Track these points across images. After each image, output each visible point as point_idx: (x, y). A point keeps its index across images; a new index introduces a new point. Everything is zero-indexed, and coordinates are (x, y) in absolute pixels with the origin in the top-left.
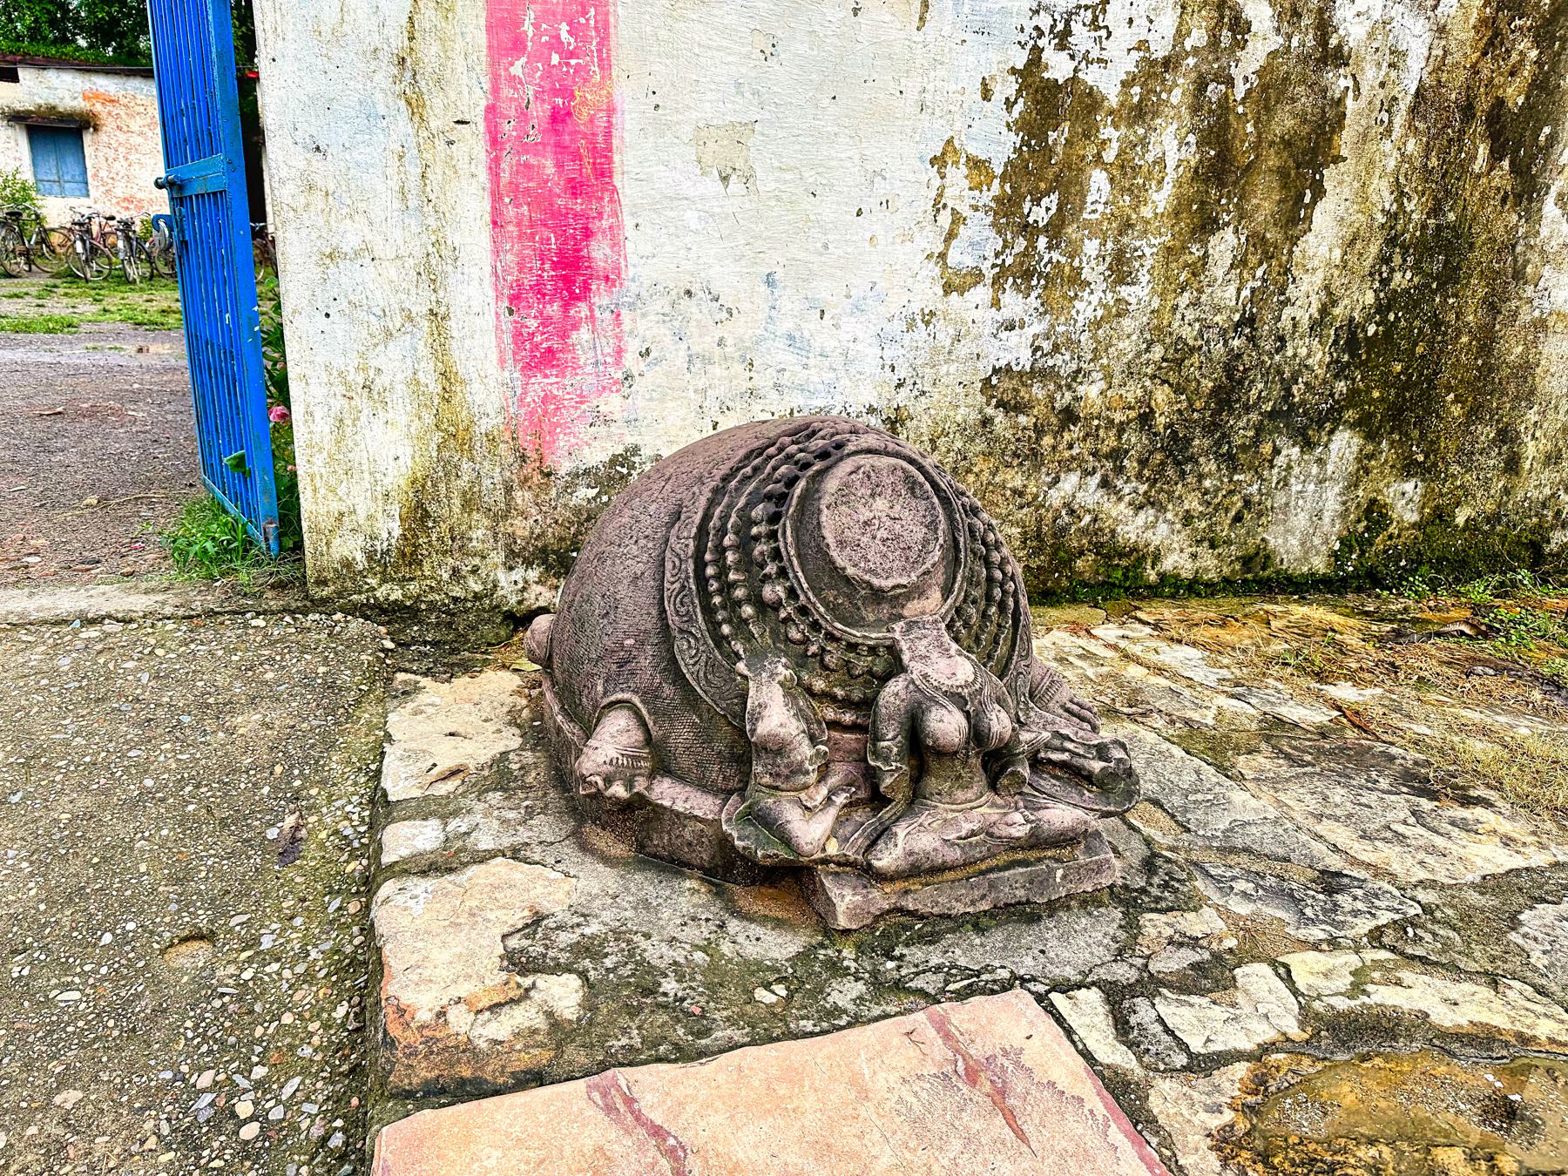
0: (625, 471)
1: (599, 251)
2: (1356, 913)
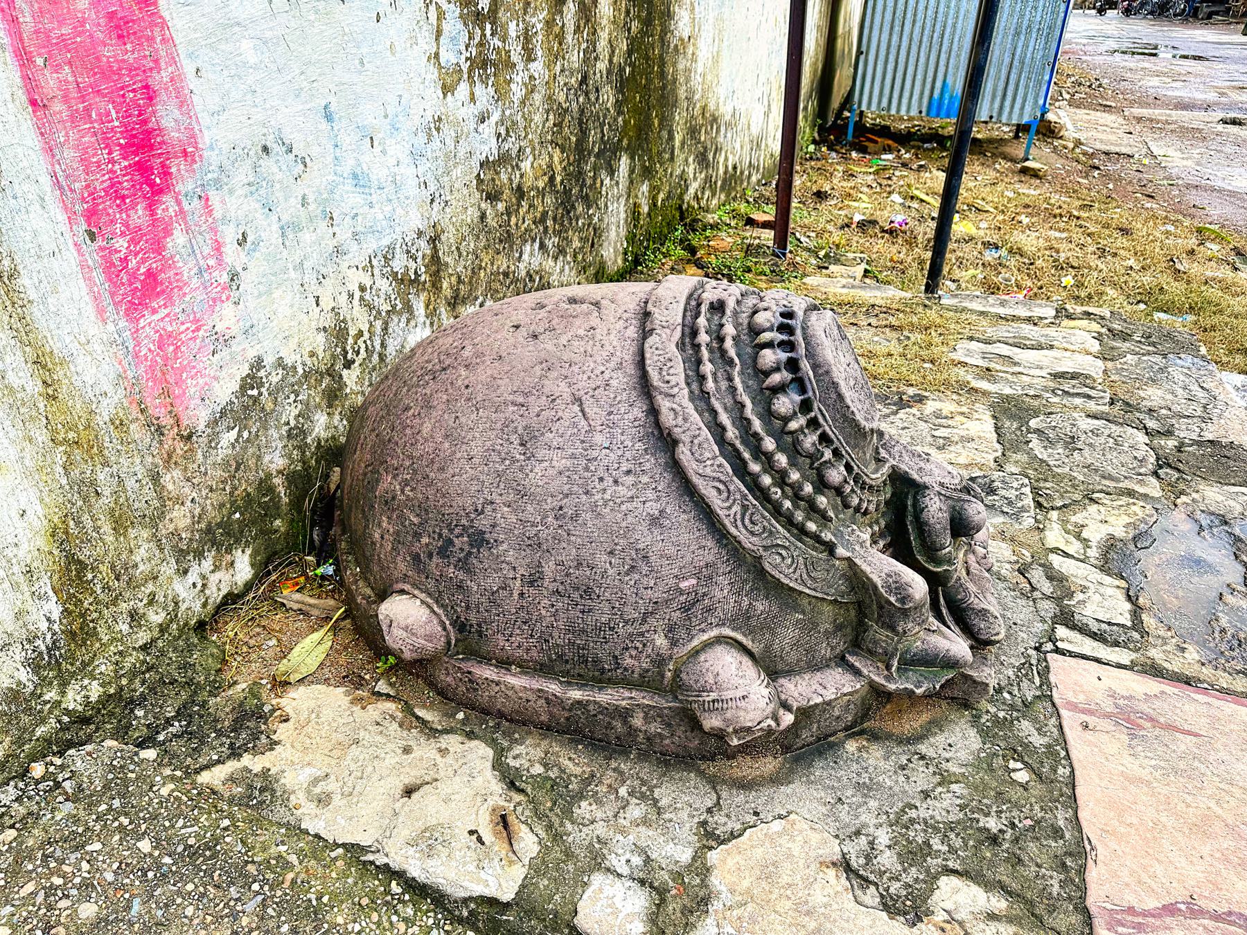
0: (255, 392)
1: (167, 117)
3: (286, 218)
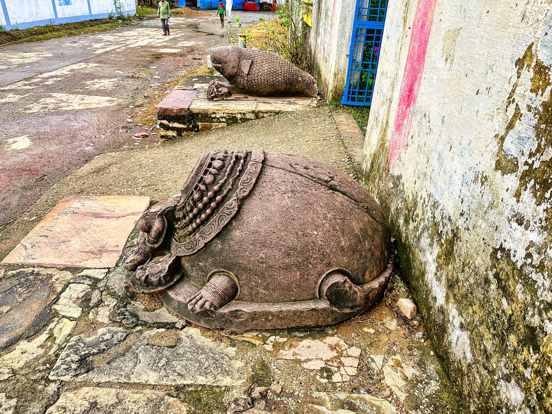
2: (68, 355)
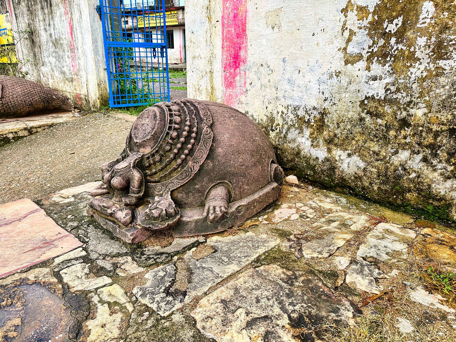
3: (263, 83)
